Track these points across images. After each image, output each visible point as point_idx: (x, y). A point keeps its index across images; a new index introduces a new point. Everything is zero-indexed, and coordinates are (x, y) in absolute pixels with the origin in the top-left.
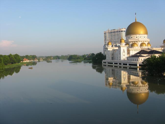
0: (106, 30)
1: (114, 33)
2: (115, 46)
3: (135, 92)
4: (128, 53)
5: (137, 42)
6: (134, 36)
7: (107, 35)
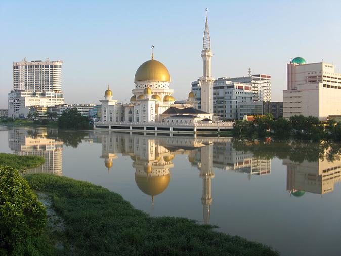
0: (20, 61)
1: (44, 69)
2: (40, 94)
3: (155, 174)
4: (156, 111)
5: (160, 93)
6: (155, 83)
7: (22, 71)
